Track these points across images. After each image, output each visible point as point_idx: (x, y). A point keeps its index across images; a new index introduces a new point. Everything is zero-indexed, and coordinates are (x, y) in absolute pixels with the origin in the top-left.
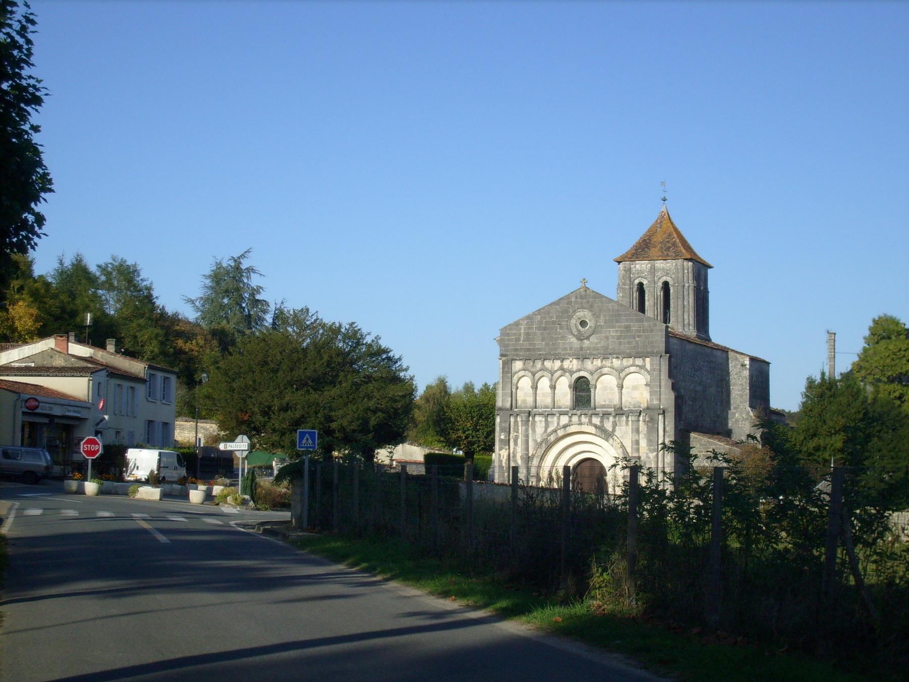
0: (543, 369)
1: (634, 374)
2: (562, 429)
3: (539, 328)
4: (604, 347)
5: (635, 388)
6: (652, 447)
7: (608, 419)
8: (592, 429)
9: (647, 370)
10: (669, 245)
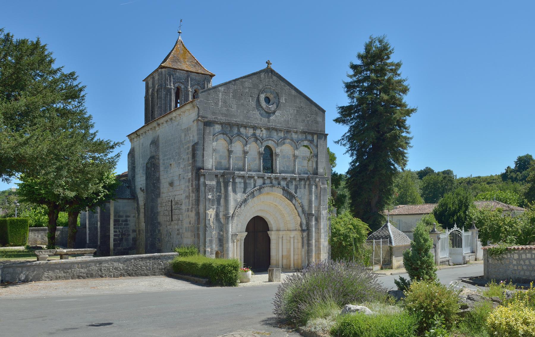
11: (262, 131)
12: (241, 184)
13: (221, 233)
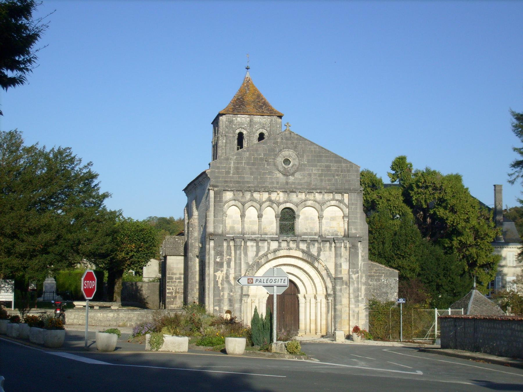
0: (253, 200)
1: (332, 207)
3: (248, 164)
4: (307, 182)
5: (333, 219)
6: (355, 270)
7: (314, 245)
8: (300, 254)
10: (261, 104)
11: (278, 194)
12: (252, 248)
13: (231, 294)
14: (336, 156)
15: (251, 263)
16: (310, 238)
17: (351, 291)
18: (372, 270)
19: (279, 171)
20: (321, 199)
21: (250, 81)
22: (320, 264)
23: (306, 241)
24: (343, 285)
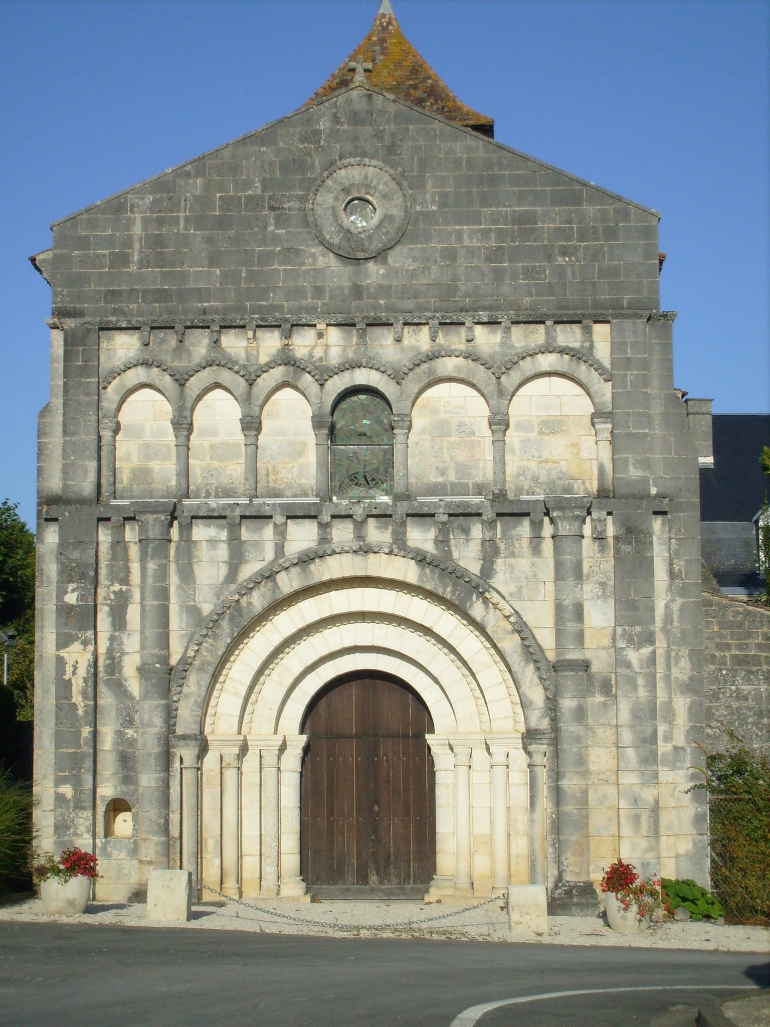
1: (546, 380)
2: (294, 571)
3: (199, 222)
6: (638, 629)
7: (466, 531)
8: (408, 571)
9: (598, 367)
10: (419, 94)
11: (320, 335)
12: (214, 548)
13: (130, 732)
14: (557, 177)
15: (207, 609)
16: (449, 505)
17: (624, 716)
18: (749, 635)
19: (322, 243)
20: (498, 349)
21: (390, 27)
22: (491, 610)
23: (433, 515)
24: (593, 694)
